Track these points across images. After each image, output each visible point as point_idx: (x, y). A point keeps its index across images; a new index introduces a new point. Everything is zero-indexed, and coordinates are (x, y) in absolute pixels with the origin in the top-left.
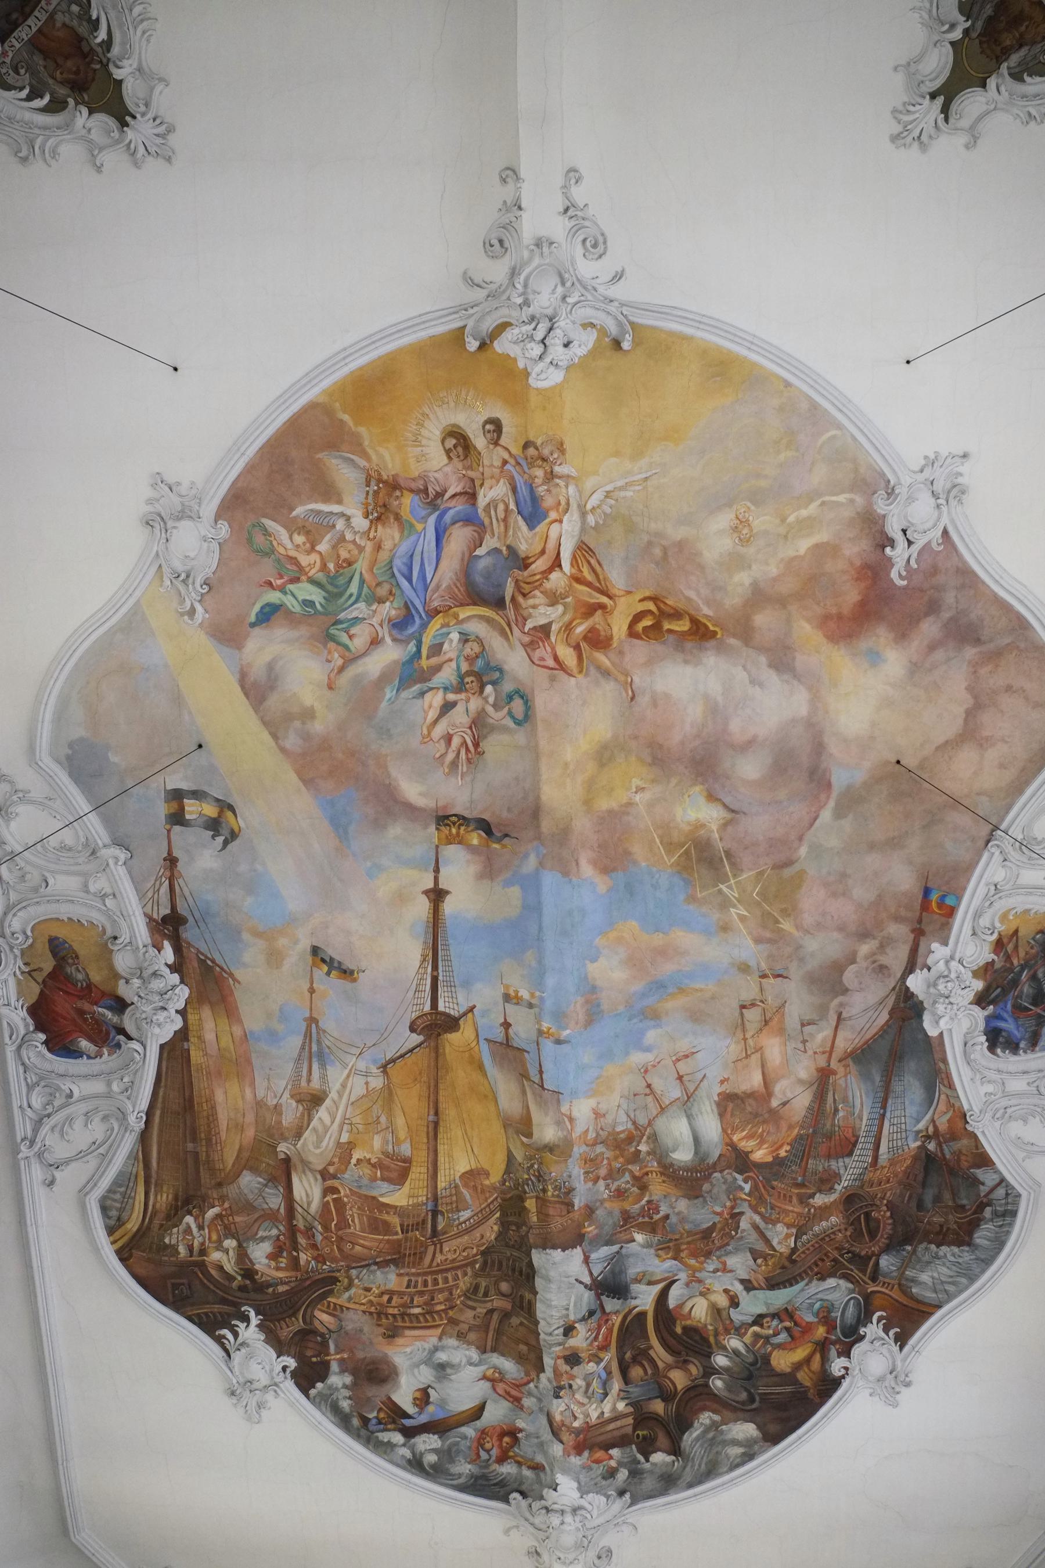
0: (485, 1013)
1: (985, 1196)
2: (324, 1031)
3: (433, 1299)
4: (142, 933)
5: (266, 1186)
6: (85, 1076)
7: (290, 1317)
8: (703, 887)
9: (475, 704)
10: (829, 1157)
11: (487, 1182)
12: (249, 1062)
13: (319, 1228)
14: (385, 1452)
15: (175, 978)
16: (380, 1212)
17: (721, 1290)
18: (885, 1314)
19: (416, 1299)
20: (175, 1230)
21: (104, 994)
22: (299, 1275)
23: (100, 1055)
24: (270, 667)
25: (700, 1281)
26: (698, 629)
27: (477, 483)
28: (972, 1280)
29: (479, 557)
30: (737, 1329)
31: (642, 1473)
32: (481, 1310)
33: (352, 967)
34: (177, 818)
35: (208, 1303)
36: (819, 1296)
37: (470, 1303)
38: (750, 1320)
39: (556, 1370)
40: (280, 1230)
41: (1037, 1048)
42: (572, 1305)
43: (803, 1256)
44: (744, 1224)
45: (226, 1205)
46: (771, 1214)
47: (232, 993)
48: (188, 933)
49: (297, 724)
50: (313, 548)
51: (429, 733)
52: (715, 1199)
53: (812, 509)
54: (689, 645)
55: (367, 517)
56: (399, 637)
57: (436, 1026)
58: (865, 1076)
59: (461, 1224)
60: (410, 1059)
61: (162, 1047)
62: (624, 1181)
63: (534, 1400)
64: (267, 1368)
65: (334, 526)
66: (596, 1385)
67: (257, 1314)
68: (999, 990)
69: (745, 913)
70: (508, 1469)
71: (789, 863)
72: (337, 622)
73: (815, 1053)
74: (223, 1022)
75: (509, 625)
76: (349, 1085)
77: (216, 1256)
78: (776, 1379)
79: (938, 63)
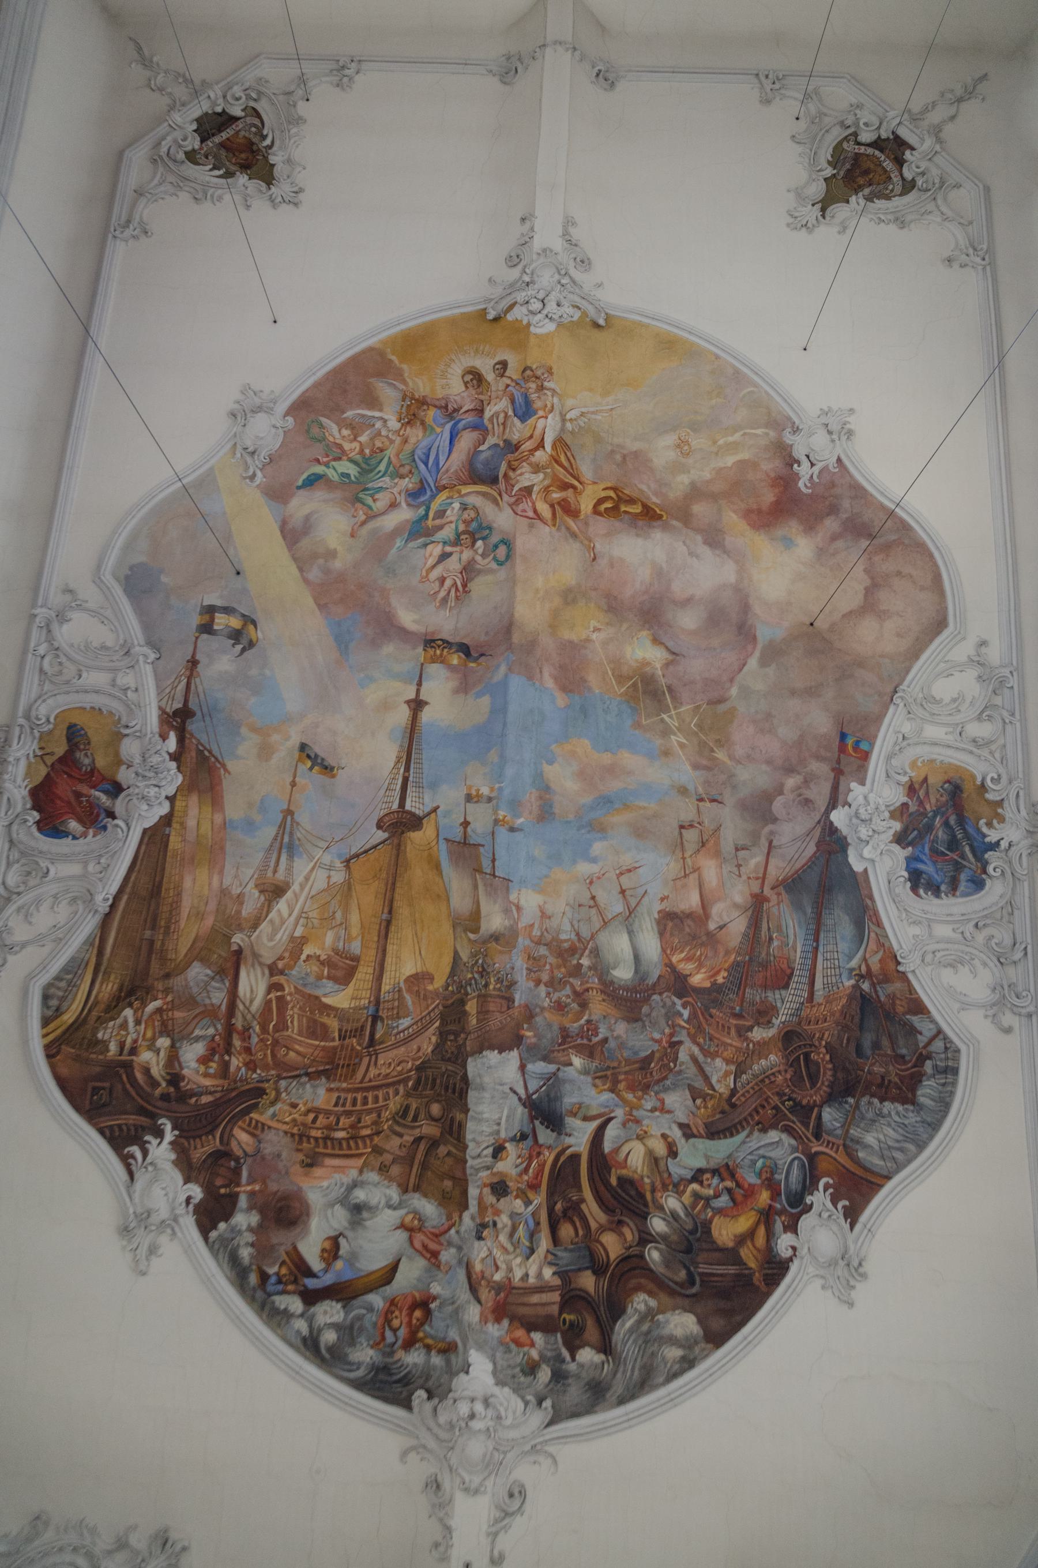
0: (447, 814)
1: (925, 1047)
2: (298, 824)
3: (359, 1121)
4: (153, 720)
5: (213, 978)
7: (207, 1134)
9: (467, 554)
10: (765, 987)
11: (430, 988)
12: (222, 849)
14: (279, 1325)
15: (173, 765)
16: (321, 1013)
17: (659, 1134)
18: (831, 1182)
19: (342, 1120)
20: (111, 1023)
21: (104, 779)
22: (226, 1083)
23: (84, 835)
24: (307, 518)
25: (637, 1122)
26: (648, 512)
28: (921, 1146)
30: (676, 1186)
31: (566, 1378)
32: (408, 1139)
33: (333, 764)
35: (126, 1113)
36: (761, 1152)
37: (397, 1128)
38: (689, 1175)
39: (482, 1207)
40: (217, 1030)
43: (743, 1099)
44: (683, 1056)
45: (169, 998)
46: (710, 1046)
47: (220, 783)
48: (193, 726)
49: (321, 561)
50: (355, 439)
52: (654, 1024)
53: (737, 437)
54: (640, 523)
56: (412, 503)
57: (401, 823)
58: (798, 906)
59: (399, 1033)
60: (373, 855)
61: (145, 831)
62: (564, 994)
64: (171, 1195)
65: (374, 425)
66: (521, 1231)
67: (174, 1129)
68: (916, 832)
69: (684, 741)
70: (414, 1358)
71: (721, 701)
73: (749, 878)
74: (208, 809)
75: (500, 495)
77: (146, 1056)
78: (717, 1255)
79: (817, 189)
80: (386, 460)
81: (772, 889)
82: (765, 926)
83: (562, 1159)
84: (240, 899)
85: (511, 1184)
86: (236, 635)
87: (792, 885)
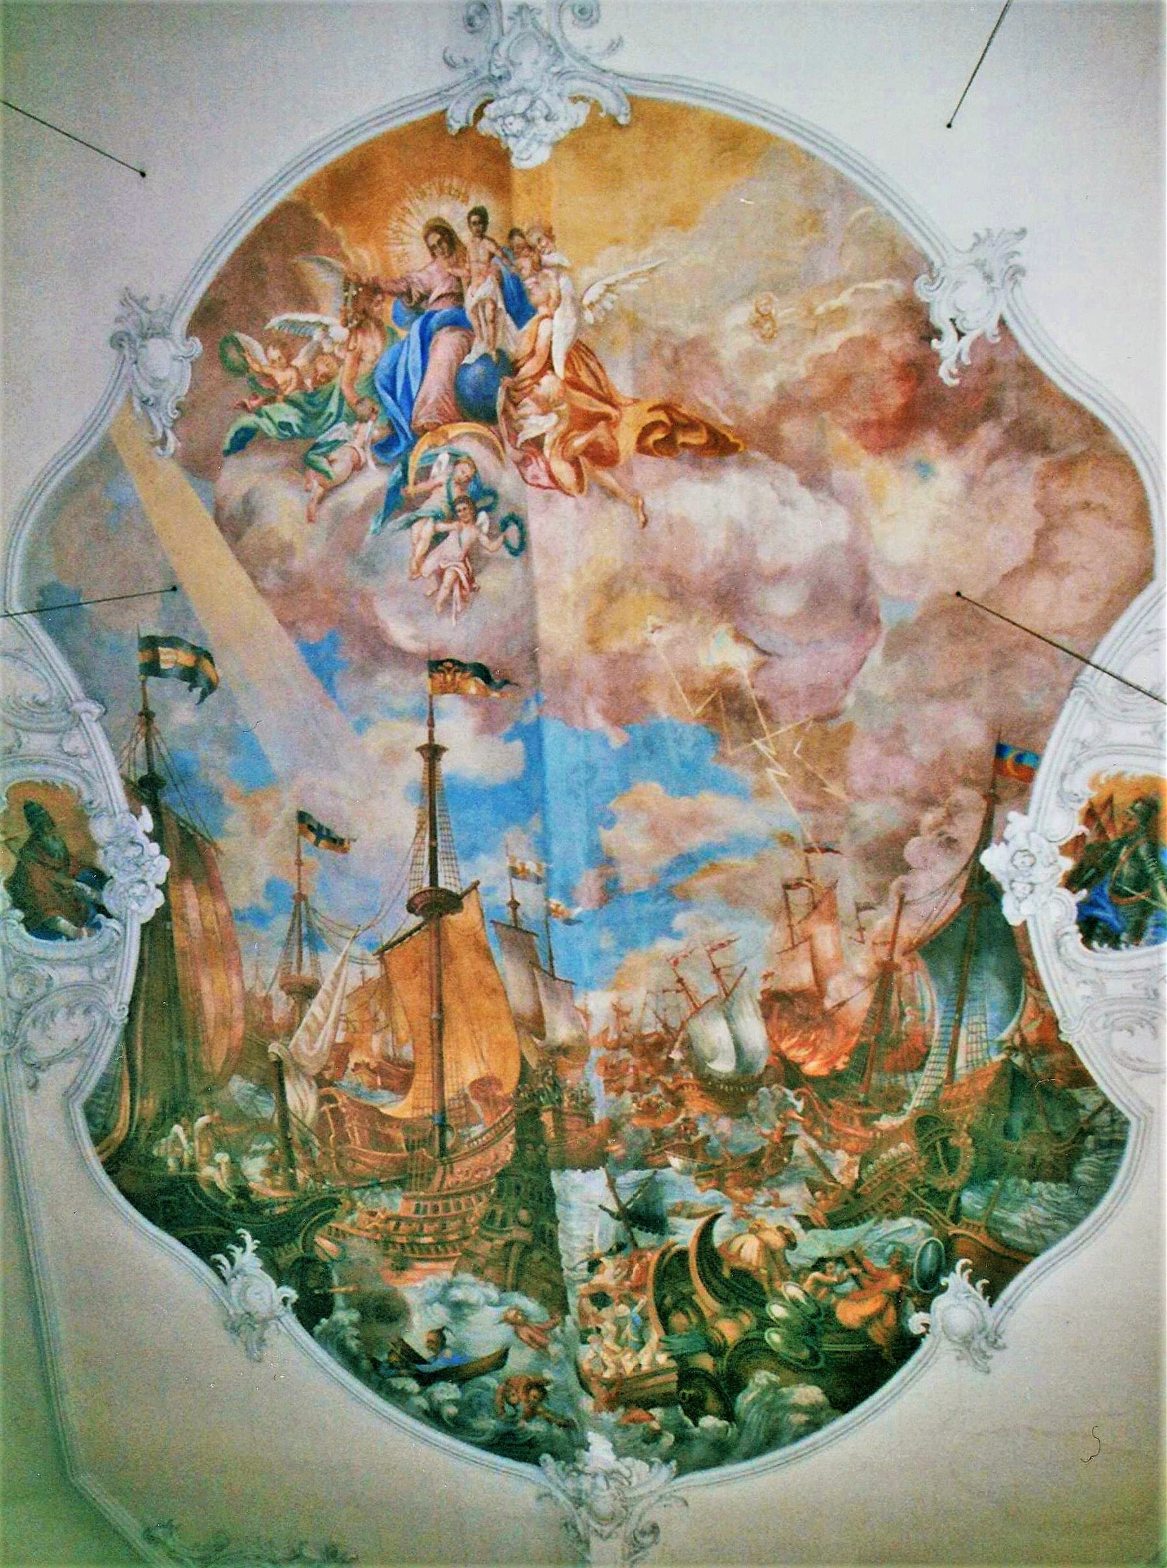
0: (491, 890)
1: (1088, 1121)
2: (315, 911)
6: (63, 961)
8: (736, 743)
9: (469, 534)
10: (896, 1070)
11: (499, 1093)
13: (317, 1142)
15: (155, 848)
22: (296, 1194)
23: (78, 936)
24: (246, 499)
27: (464, 282)
28: (1074, 1222)
29: (467, 366)
32: (499, 1242)
34: (152, 668)
36: (890, 1239)
38: (810, 1264)
39: (583, 1315)
41: (1142, 942)
42: (596, 1235)
44: (798, 1149)
45: (216, 1114)
49: (276, 561)
50: (288, 365)
51: (419, 566)
52: (762, 1119)
53: (845, 298)
55: (345, 325)
57: (437, 904)
58: (935, 974)
63: (560, 1346)
65: (310, 338)
66: (629, 1331)
67: (254, 1238)
68: (1093, 871)
71: (834, 715)
72: (316, 446)
73: (874, 943)
74: (207, 899)
75: (502, 442)
76: (343, 977)
77: (207, 1171)
80: (336, 393)
81: (904, 954)
82: (894, 998)
83: (667, 1257)
84: (267, 1002)
85: (611, 1294)
86: (190, 675)
87: (930, 948)
